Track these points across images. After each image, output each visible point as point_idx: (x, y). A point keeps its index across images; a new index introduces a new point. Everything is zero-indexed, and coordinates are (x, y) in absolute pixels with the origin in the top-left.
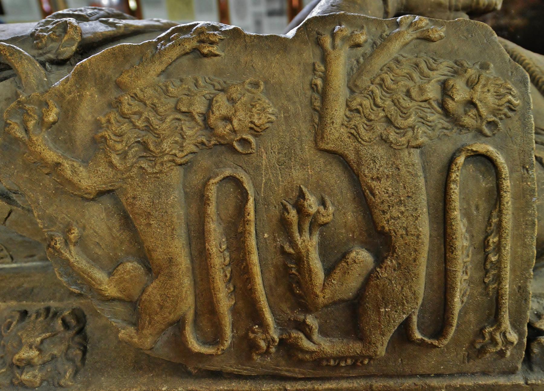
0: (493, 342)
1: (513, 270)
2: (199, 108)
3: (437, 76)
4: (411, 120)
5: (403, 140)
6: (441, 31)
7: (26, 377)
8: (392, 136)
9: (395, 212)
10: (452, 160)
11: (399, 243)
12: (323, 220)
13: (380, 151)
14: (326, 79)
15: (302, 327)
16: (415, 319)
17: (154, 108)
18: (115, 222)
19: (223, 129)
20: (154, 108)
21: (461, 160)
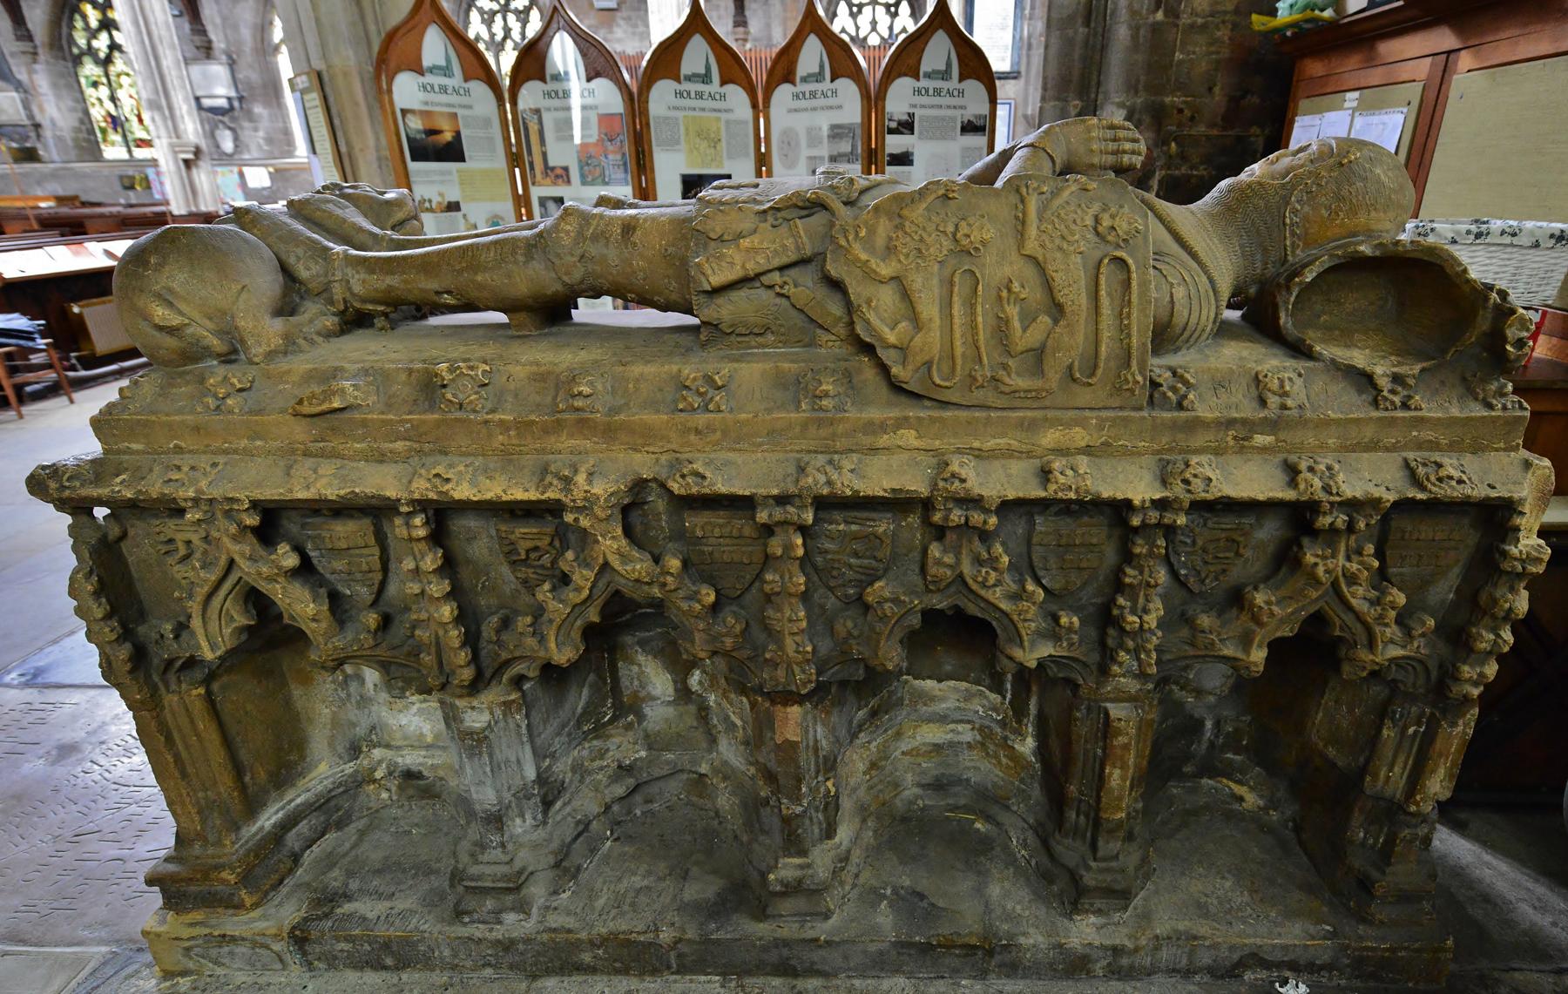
0: (1127, 381)
1: (1139, 331)
2: (950, 229)
3: (1091, 212)
4: (1076, 237)
5: (1072, 248)
6: (1095, 185)
7: (824, 402)
8: (1065, 246)
9: (1066, 291)
10: (1101, 261)
11: (1068, 310)
12: (1023, 296)
13: (1058, 255)
14: (1024, 213)
15: (1005, 367)
16: (1076, 363)
17: (924, 229)
18: (897, 297)
19: (965, 242)
20: (924, 229)
21: (1106, 261)
